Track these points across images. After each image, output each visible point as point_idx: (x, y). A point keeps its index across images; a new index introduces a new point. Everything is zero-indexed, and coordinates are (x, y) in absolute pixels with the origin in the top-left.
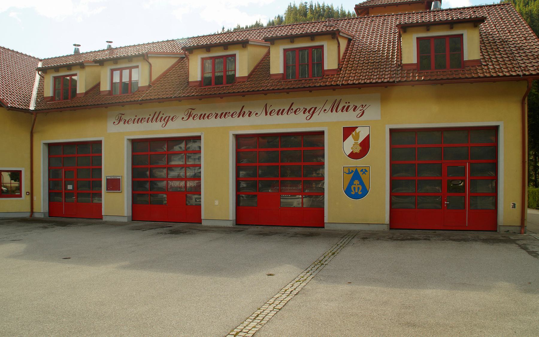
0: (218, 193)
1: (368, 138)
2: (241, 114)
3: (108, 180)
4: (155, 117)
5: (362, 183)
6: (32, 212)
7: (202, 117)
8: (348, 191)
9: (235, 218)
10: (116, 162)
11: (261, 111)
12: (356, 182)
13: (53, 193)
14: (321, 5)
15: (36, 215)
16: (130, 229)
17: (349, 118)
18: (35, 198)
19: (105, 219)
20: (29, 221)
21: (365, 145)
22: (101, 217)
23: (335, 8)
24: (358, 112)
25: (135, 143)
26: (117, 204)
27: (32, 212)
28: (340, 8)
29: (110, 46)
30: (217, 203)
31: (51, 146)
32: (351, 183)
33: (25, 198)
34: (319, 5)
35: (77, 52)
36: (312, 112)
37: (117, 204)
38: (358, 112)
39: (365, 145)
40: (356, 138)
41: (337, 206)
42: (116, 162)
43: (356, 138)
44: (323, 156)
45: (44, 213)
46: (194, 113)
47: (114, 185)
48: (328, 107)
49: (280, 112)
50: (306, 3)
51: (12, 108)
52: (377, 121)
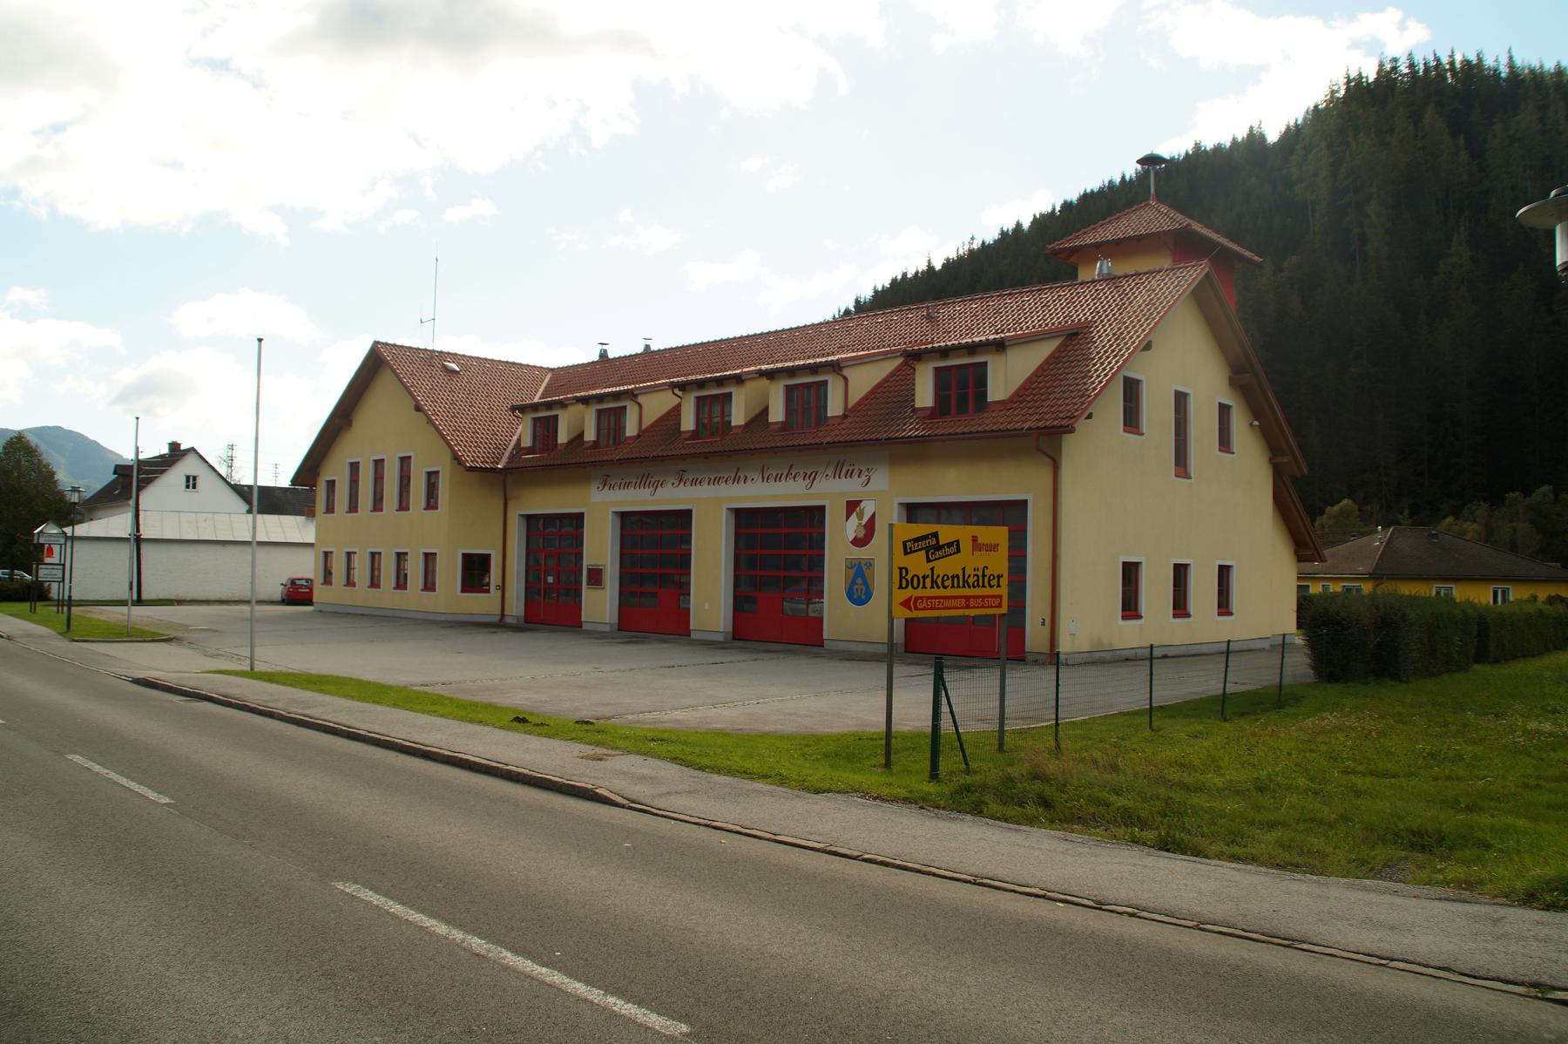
0: (711, 589)
1: (873, 516)
2: (736, 480)
3: (589, 570)
4: (644, 480)
5: (865, 583)
6: (503, 615)
7: (694, 482)
8: (850, 595)
9: (730, 629)
10: (601, 547)
11: (757, 476)
12: (859, 581)
13: (531, 588)
14: (1445, 60)
15: (508, 620)
16: (1529, 899)
17: (849, 487)
18: (507, 595)
19: (585, 627)
20: (500, 625)
21: (870, 526)
22: (580, 624)
23: (1489, 62)
24: (864, 478)
25: (624, 516)
26: (600, 604)
27: (503, 615)
28: (1504, 61)
29: (647, 347)
30: (707, 606)
31: (530, 519)
32: (854, 582)
33: (494, 594)
34: (1437, 59)
35: (603, 355)
36: (812, 477)
37: (600, 604)
38: (864, 478)
39: (870, 526)
40: (860, 517)
41: (837, 613)
42: (601, 547)
43: (860, 517)
44: (689, 542)
45: (518, 617)
46: (686, 476)
47: (596, 577)
48: (830, 472)
49: (778, 478)
50: (1395, 60)
51: (471, 469)
52: (884, 491)
